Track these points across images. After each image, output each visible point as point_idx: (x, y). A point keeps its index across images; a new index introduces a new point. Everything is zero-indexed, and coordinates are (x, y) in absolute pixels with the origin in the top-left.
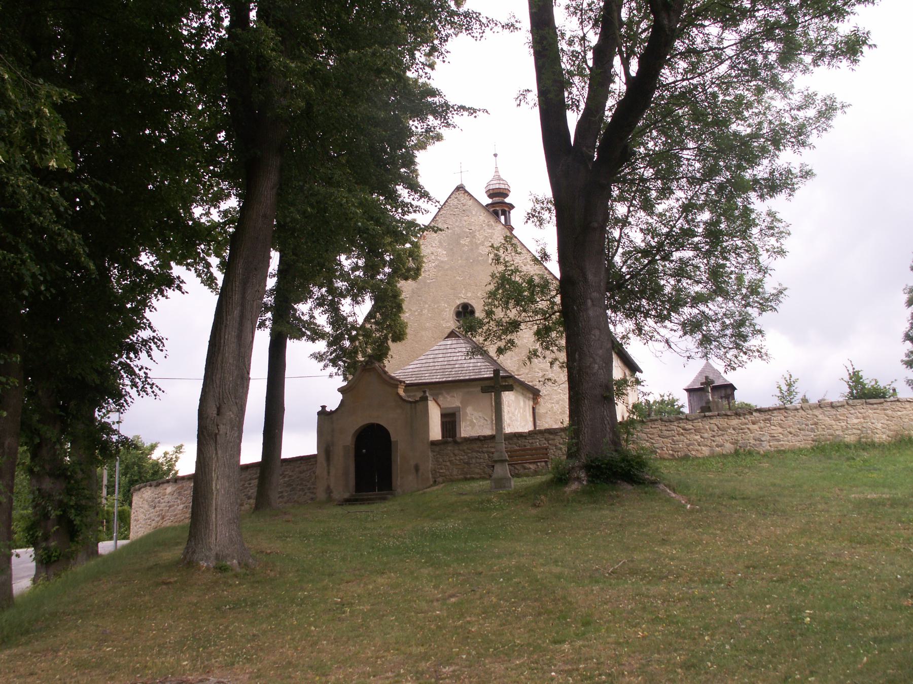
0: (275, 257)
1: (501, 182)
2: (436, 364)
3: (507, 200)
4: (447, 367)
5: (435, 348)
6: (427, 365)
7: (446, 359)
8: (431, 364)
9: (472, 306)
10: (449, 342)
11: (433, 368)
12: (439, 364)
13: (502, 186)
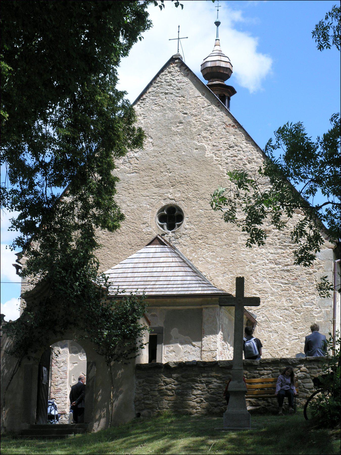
0: (340, 241)
1: (223, 59)
2: (136, 275)
3: (227, 83)
4: (149, 279)
5: (134, 256)
6: (125, 275)
7: (148, 270)
8: (129, 275)
9: (180, 210)
10: (153, 250)
11: (131, 279)
12: (140, 275)
13: (223, 65)
